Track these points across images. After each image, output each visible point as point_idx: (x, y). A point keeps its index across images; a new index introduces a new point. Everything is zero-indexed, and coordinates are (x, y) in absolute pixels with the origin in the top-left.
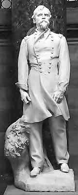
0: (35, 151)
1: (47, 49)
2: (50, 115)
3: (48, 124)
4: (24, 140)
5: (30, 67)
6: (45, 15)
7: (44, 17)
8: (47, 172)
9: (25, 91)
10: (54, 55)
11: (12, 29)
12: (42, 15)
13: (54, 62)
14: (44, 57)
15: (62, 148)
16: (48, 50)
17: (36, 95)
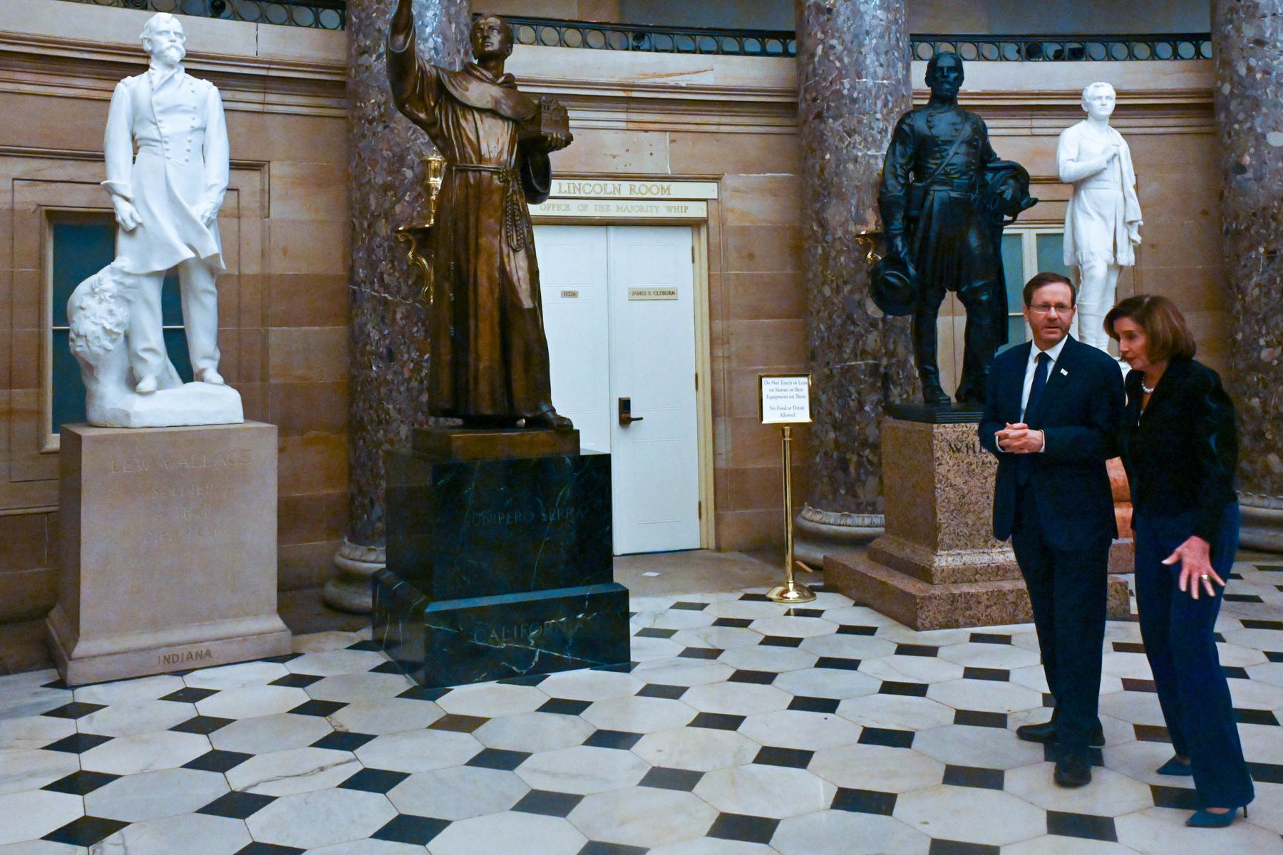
0: (146, 339)
1: (182, 108)
2: (191, 255)
3: (182, 278)
4: (122, 313)
5: (136, 150)
6: (175, 33)
7: (174, 37)
8: (171, 388)
9: (127, 199)
10: (197, 123)
11: (854, 371)
12: (168, 32)
13: (196, 138)
14: (171, 126)
15: (521, 268)
16: (185, 111)
17: (156, 209)
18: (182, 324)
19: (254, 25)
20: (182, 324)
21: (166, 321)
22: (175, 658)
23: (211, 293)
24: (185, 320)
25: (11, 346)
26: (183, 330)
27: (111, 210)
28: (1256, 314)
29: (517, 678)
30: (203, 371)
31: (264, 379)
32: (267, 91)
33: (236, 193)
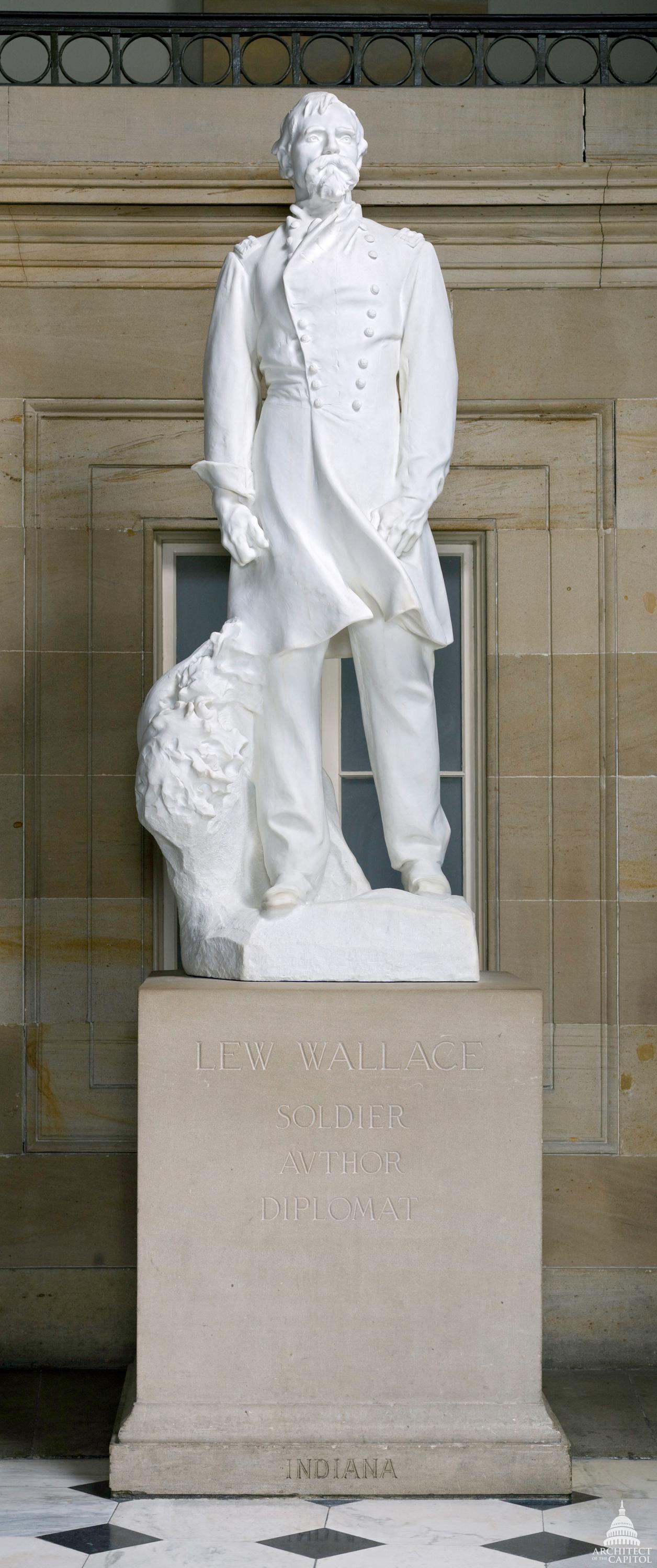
18: (370, 769)
19: (577, 92)
20: (370, 769)
21: (443, 766)
22: (322, 1469)
23: (419, 696)
24: (372, 765)
25: (216, 833)
26: (370, 781)
27: (438, 538)
28: (152, 488)
29: (114, 1499)
30: (409, 864)
31: (607, 889)
32: (608, 238)
33: (541, 474)
